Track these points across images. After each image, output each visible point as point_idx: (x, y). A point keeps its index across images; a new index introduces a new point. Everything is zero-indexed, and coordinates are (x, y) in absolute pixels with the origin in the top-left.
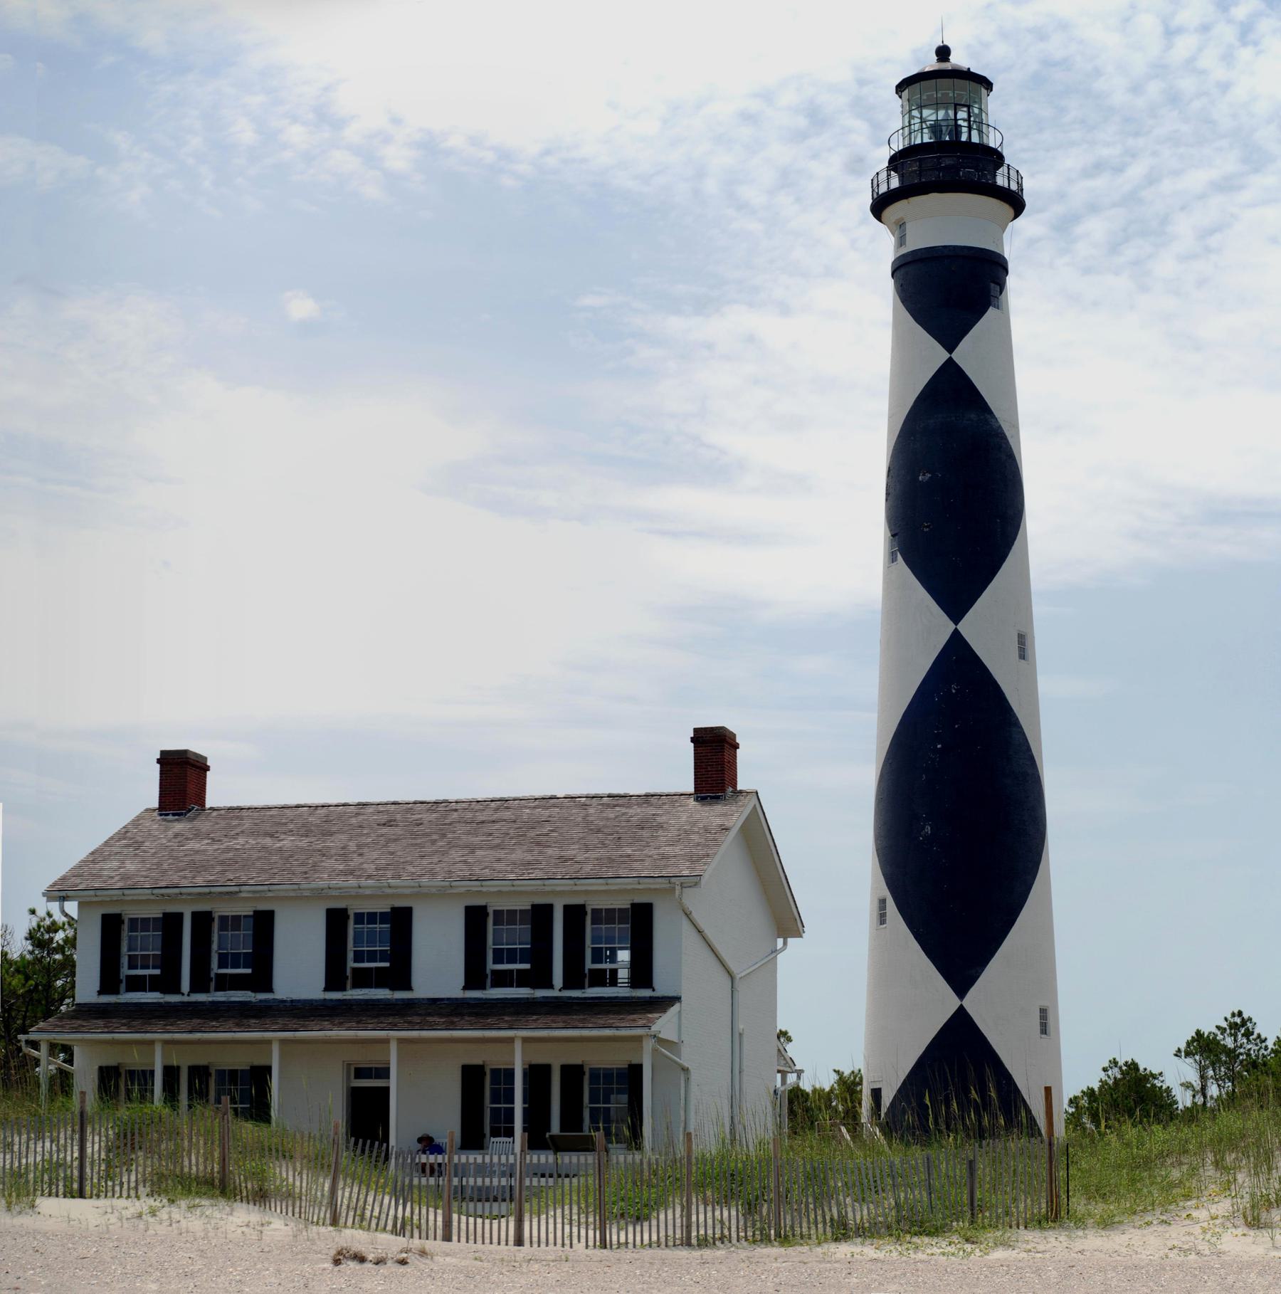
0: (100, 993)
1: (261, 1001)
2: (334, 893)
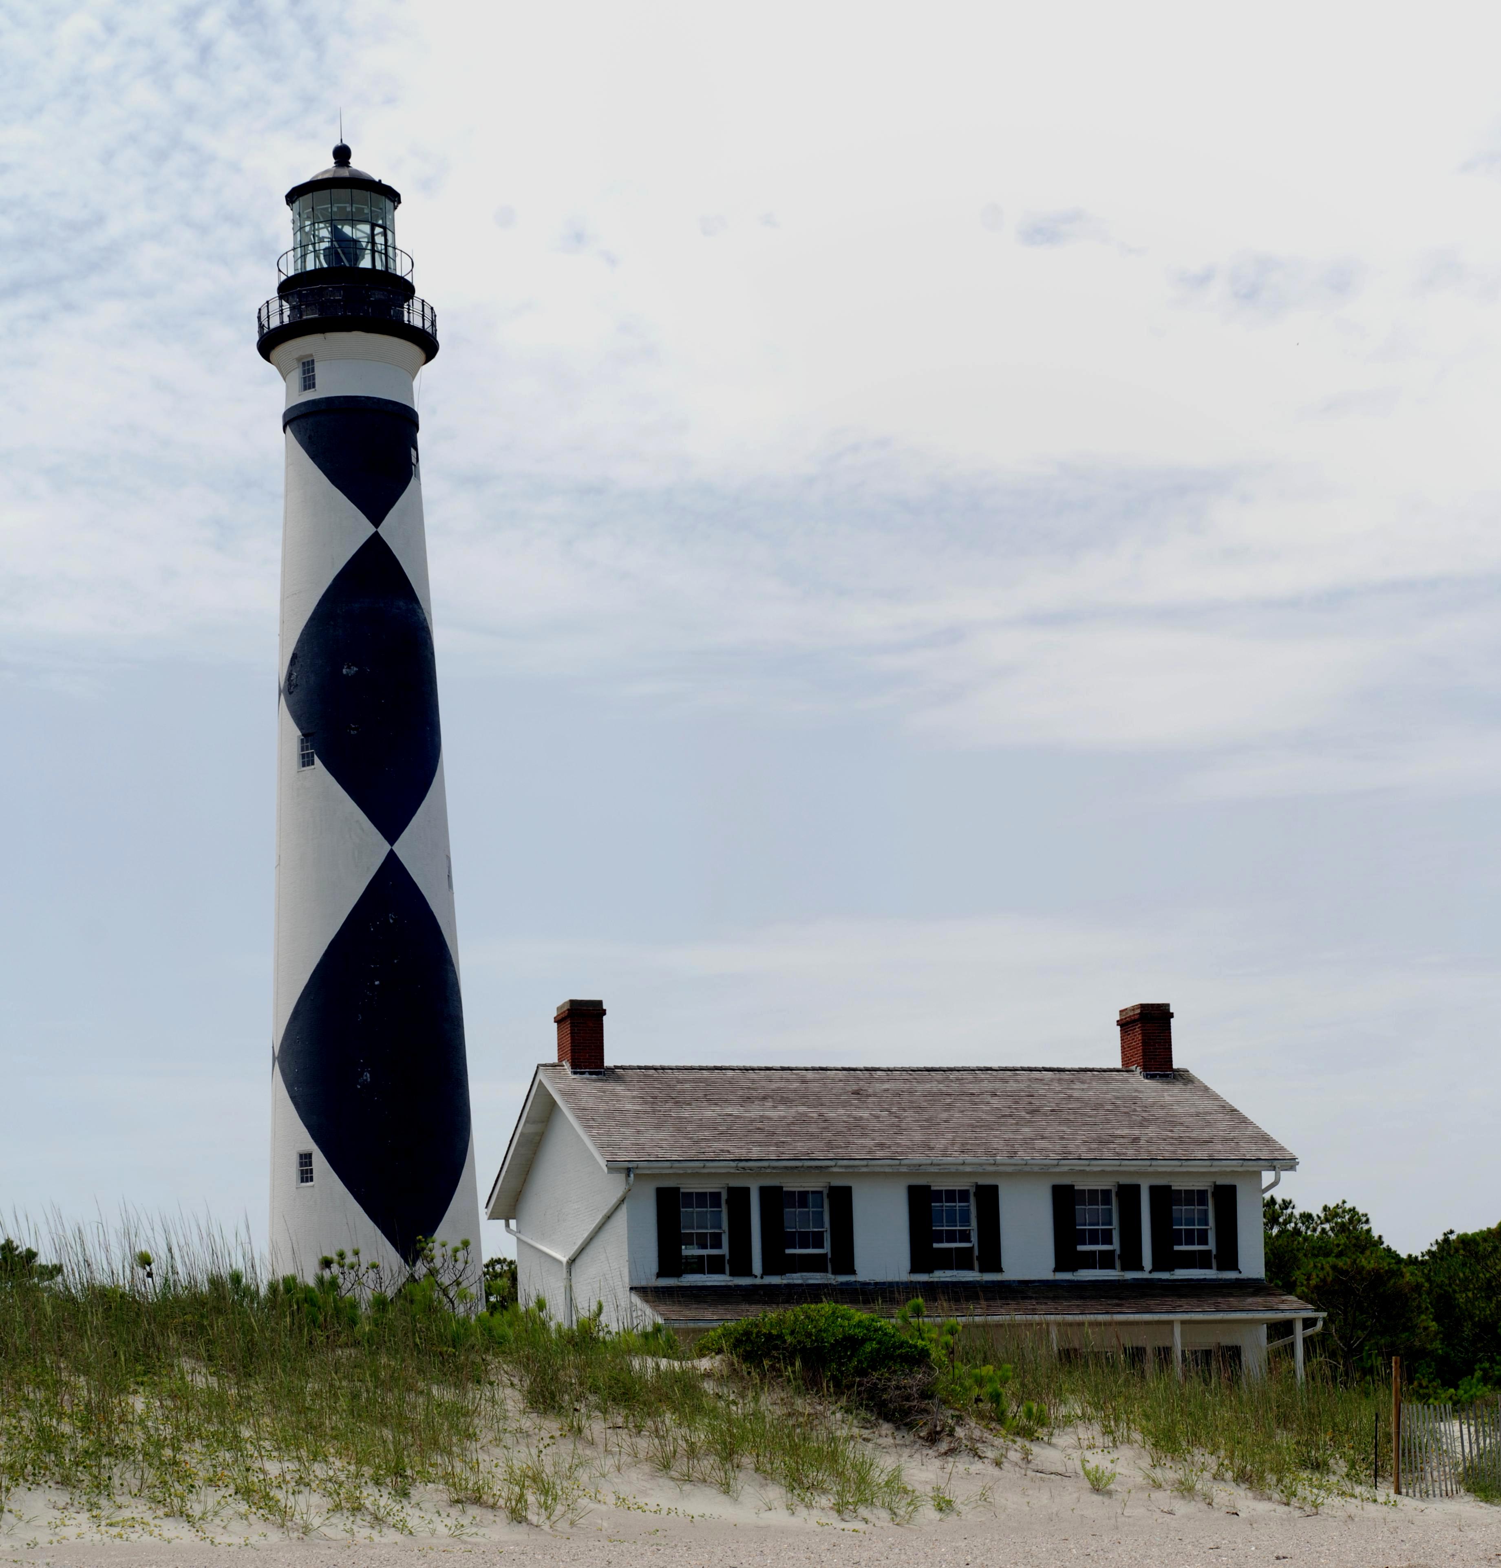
0: (659, 1275)
1: (842, 1284)
2: (968, 1169)
